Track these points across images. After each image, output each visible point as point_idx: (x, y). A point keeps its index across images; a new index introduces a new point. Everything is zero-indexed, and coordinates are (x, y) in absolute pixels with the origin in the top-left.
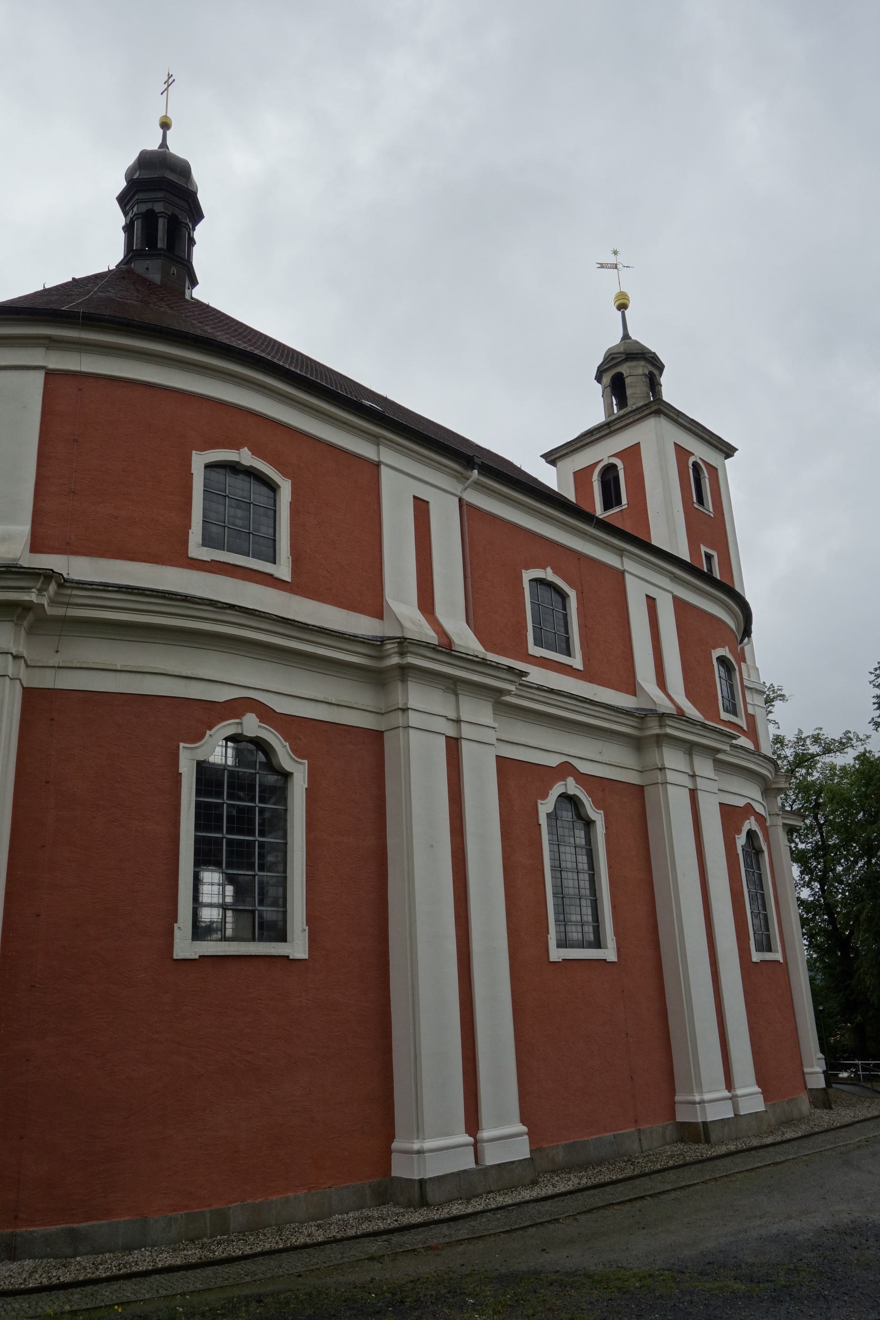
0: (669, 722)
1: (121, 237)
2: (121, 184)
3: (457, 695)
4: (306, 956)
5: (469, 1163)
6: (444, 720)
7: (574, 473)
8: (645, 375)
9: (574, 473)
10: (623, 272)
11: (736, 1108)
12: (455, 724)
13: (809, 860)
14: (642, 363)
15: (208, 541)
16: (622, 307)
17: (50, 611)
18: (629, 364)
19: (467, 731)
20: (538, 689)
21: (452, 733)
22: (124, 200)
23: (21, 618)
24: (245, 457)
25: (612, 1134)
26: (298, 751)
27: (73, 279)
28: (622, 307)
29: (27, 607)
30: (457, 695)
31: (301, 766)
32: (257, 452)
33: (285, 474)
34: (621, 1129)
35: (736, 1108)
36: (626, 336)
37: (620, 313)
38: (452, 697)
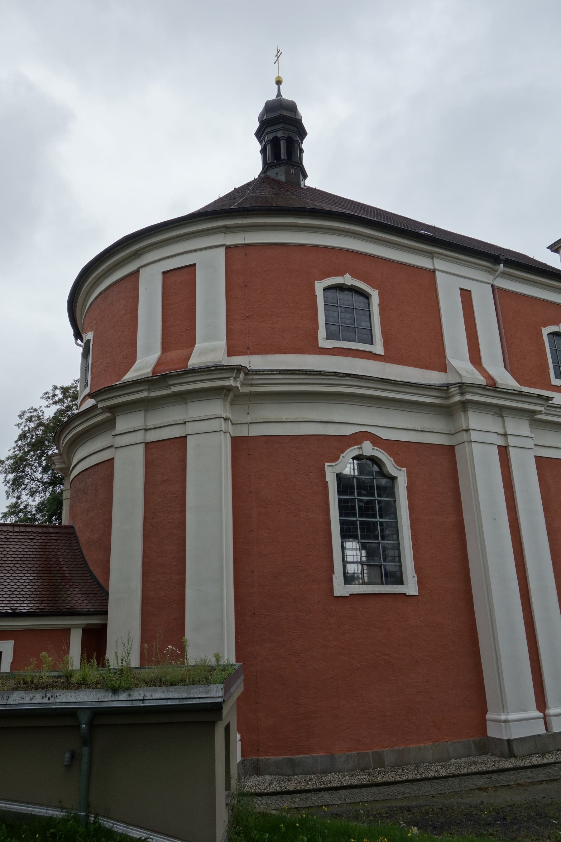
3: (502, 417)
6: (495, 435)
12: (503, 437)
15: (330, 336)
17: (242, 390)
19: (512, 441)
21: (501, 443)
23: (226, 395)
24: (348, 280)
26: (399, 463)
29: (228, 389)
32: (355, 276)
38: (500, 419)
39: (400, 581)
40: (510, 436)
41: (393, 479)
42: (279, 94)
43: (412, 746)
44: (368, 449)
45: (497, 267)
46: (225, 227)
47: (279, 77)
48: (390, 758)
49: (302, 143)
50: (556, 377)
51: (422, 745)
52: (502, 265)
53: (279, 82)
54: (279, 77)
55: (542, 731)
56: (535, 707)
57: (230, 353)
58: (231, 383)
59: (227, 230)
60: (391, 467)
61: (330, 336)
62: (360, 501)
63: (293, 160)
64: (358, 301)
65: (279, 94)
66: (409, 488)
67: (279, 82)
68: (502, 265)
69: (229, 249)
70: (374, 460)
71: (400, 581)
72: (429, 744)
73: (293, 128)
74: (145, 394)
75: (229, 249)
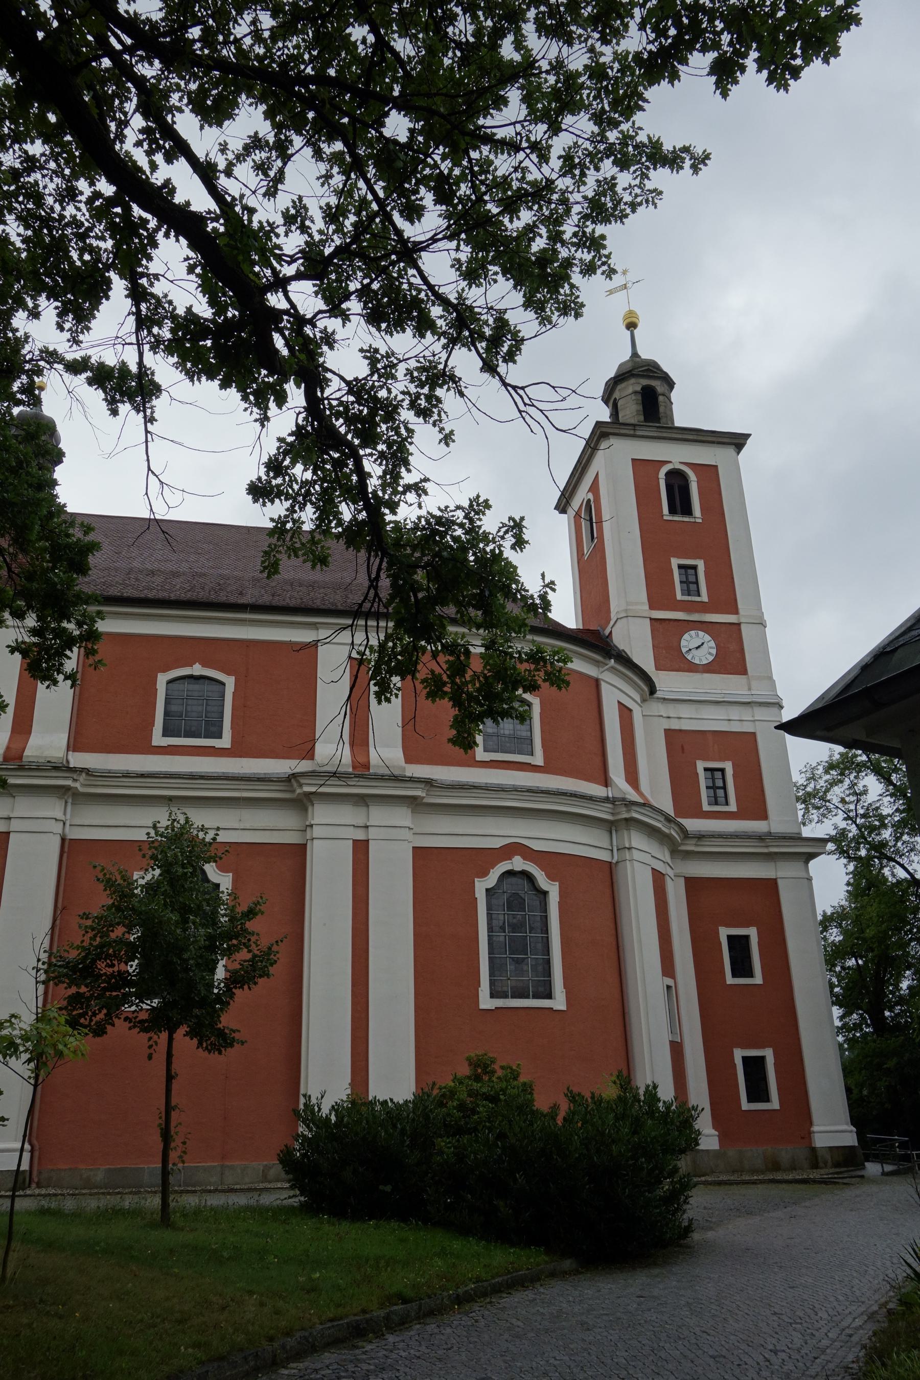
0: (302, 781)
3: (368, 806)
7: (716, 467)
8: (635, 392)
9: (716, 467)
10: (633, 290)
12: (363, 829)
14: (633, 381)
15: (166, 733)
16: (631, 326)
17: (81, 789)
18: (619, 387)
19: (373, 833)
20: (123, 776)
21: (360, 835)
23: (64, 794)
24: (197, 669)
26: (551, 877)
27: (840, 47)
28: (631, 326)
29: (67, 789)
32: (205, 665)
36: (635, 354)
37: (629, 332)
38: (365, 809)
39: (549, 996)
41: (545, 893)
44: (518, 863)
45: (607, 662)
52: (613, 661)
57: (75, 744)
58: (69, 783)
60: (542, 881)
61: (166, 733)
63: (680, 421)
64: (216, 687)
66: (560, 904)
68: (613, 661)
70: (526, 875)
71: (549, 996)
74: (659, 825)
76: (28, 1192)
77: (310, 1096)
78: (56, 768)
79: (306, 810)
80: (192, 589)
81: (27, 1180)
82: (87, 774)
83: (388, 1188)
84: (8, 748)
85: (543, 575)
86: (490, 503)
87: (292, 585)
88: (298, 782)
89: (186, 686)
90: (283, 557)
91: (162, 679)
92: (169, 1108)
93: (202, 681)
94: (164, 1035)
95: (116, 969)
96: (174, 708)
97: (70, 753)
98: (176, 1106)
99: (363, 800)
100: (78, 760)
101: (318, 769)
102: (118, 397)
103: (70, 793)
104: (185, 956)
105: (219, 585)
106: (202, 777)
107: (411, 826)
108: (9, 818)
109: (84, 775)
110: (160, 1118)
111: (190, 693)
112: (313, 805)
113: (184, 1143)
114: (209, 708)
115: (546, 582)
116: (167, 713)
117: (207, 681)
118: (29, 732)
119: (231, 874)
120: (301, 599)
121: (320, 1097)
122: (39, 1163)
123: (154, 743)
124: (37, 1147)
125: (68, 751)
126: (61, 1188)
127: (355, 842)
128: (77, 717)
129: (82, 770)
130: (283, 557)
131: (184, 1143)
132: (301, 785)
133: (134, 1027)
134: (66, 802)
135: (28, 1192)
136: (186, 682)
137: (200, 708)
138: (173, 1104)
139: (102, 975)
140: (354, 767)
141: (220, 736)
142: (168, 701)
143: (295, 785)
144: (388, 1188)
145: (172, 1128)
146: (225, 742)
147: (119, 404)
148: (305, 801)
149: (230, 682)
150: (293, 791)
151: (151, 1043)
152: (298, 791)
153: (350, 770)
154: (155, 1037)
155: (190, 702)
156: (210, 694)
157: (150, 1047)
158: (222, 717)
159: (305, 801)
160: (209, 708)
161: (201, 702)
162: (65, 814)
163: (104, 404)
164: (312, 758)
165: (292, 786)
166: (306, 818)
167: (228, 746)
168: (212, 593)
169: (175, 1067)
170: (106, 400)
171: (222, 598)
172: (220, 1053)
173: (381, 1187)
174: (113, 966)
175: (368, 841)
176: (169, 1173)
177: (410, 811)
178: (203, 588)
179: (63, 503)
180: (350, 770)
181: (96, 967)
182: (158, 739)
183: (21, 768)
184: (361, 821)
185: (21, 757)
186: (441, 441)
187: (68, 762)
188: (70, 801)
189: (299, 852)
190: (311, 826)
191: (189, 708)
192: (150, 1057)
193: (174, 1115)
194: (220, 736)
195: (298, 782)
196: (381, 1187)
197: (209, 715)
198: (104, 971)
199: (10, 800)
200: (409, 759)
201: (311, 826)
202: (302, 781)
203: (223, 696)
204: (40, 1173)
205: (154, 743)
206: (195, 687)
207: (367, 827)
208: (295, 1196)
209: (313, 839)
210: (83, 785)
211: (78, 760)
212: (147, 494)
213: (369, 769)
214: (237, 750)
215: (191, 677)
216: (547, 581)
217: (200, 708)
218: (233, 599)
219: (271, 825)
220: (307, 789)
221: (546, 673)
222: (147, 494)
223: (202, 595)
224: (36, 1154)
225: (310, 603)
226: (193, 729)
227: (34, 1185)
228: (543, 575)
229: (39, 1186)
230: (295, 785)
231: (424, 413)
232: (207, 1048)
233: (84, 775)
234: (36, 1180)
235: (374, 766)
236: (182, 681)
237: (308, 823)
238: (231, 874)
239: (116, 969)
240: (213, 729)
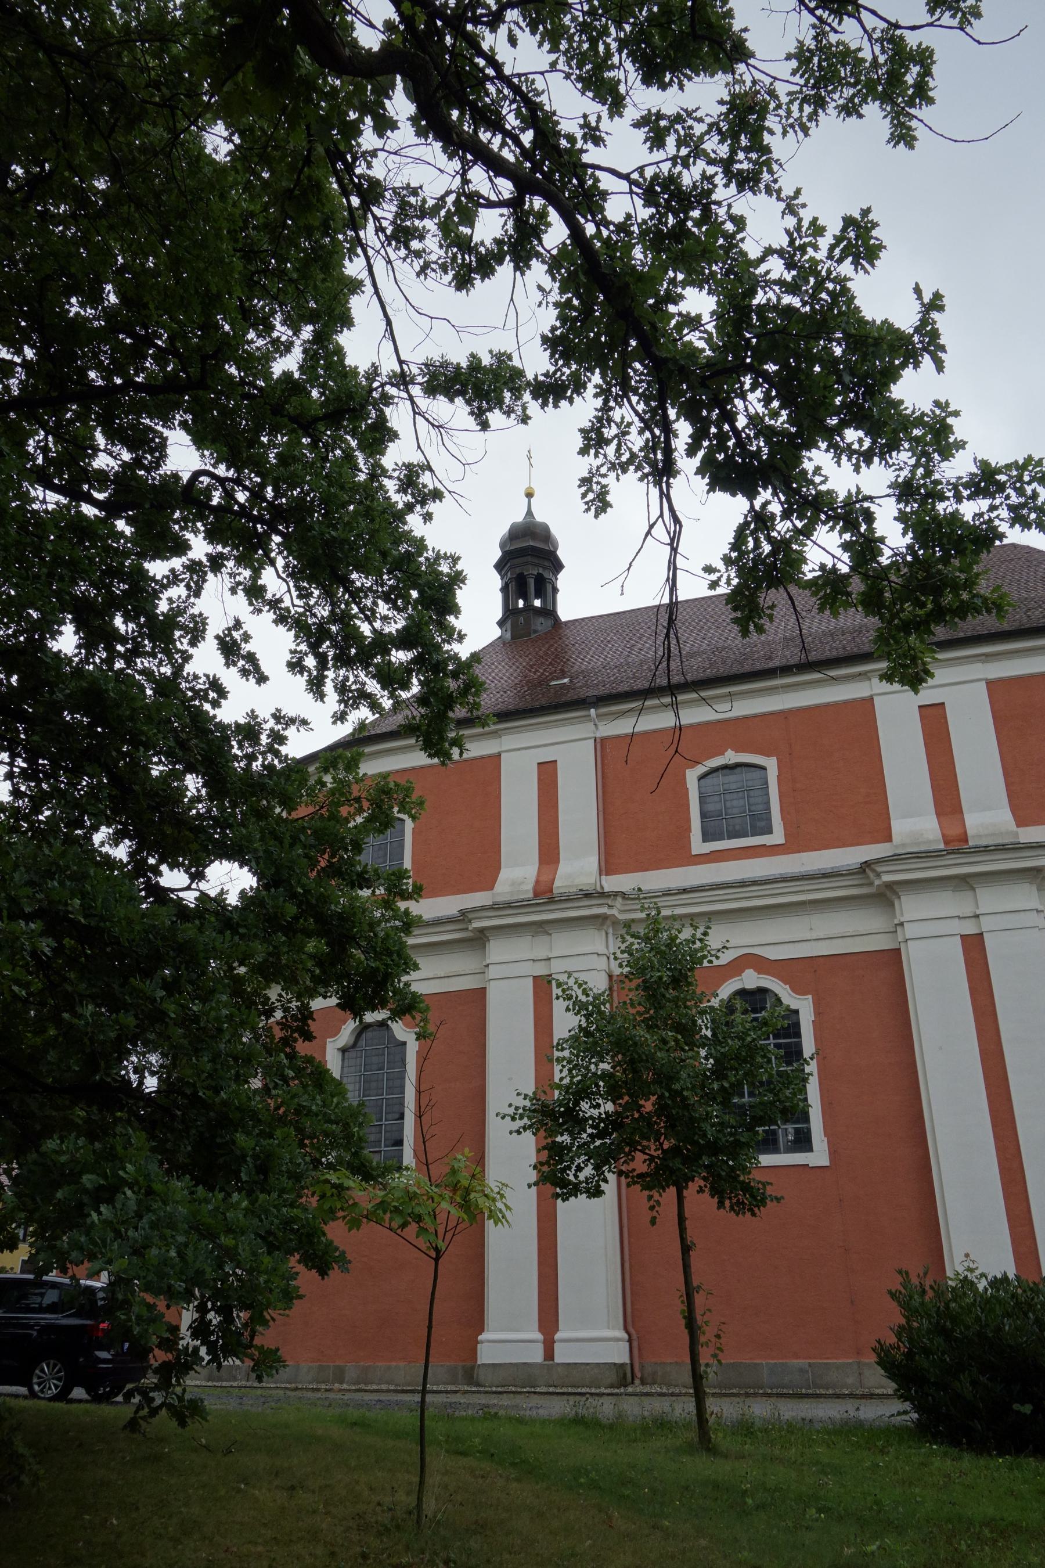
0: (879, 869)
1: (499, 597)
2: (498, 554)
3: (974, 889)
4: (828, 1164)
5: (536, 1356)
6: (957, 919)
11: (549, 1354)
12: (973, 920)
13: (720, 347)
15: (707, 837)
17: (621, 917)
19: (986, 924)
21: (970, 928)
22: (499, 566)
23: (602, 924)
24: (731, 757)
25: (808, 1361)
26: (798, 990)
30: (974, 889)
31: (805, 1002)
33: (768, 754)
34: (828, 1358)
35: (549, 1354)
38: (970, 893)
40: (910, 924)
42: (529, 513)
43: (380, 1364)
46: (986, 655)
47: (530, 487)
48: (351, 1373)
49: (557, 579)
50: (491, 888)
51: (394, 1364)
53: (529, 495)
54: (530, 487)
55: (536, 1356)
56: (536, 1325)
57: (607, 867)
58: (604, 910)
59: (988, 657)
60: (789, 998)
61: (707, 837)
62: (777, 1046)
64: (756, 774)
65: (529, 513)
67: (529, 495)
69: (992, 686)
72: (402, 1364)
73: (546, 563)
75: (992, 686)
76: (630, 1389)
77: (907, 1273)
78: (587, 895)
79: (892, 905)
80: (712, 665)
81: (629, 1375)
82: (624, 898)
83: (1027, 1409)
84: (537, 882)
85: (918, 290)
86: (820, 222)
87: (832, 635)
88: (874, 871)
89: (719, 779)
90: (610, 480)
91: (692, 776)
92: (690, 1292)
93: (739, 770)
94: (672, 1190)
95: (602, 1110)
96: (710, 807)
97: (603, 877)
98: (699, 1287)
99: (965, 882)
100: (612, 883)
101: (898, 852)
102: (484, 404)
103: (608, 922)
104: (677, 1086)
105: (744, 654)
106: (754, 883)
107: (1040, 908)
108: (549, 959)
109: (619, 899)
110: (683, 1302)
111: (726, 787)
112: (899, 898)
113: (718, 1336)
114: (752, 800)
115: (926, 300)
116: (704, 815)
117: (744, 769)
118: (557, 861)
119: (810, 996)
120: (844, 648)
121: (921, 1275)
122: (640, 1356)
123: (695, 851)
124: (634, 1336)
125: (600, 875)
126: (669, 1385)
127: (964, 938)
128: (605, 837)
129: (616, 894)
130: (610, 480)
131: (718, 1336)
132: (878, 875)
133: (635, 1183)
134: (607, 934)
135: (630, 1389)
136: (720, 773)
137: (741, 802)
138: (695, 1284)
139: (586, 1120)
140: (946, 843)
141: (769, 831)
142: (702, 799)
143: (871, 875)
144: (1027, 1409)
145: (699, 1318)
146: (777, 836)
147: (488, 414)
148: (888, 893)
149: (771, 764)
150: (871, 884)
151: (652, 1203)
152: (877, 882)
153: (942, 846)
154: (656, 1196)
155: (728, 797)
156: (750, 783)
157: (652, 1208)
158: (769, 808)
159: (888, 893)
160: (752, 800)
161: (740, 794)
162: (607, 947)
163: (472, 419)
164: (889, 838)
165: (868, 877)
166: (894, 916)
167: (782, 841)
168: (735, 664)
169: (692, 1233)
170: (472, 413)
171: (747, 667)
172: (754, 1214)
173: (1016, 1407)
174: (598, 1106)
175: (982, 934)
176: (701, 1377)
177: (1034, 888)
178: (724, 663)
179: (419, 536)
180: (942, 846)
181: (580, 1110)
182: (698, 846)
183: (551, 901)
184: (968, 911)
185: (551, 891)
186: (783, 213)
187: (602, 887)
188: (611, 931)
189: (893, 957)
190: (902, 924)
191: (728, 804)
192: (653, 1221)
193: (699, 1299)
194: (769, 831)
195: (874, 871)
196: (1016, 1407)
197: (753, 808)
198: (589, 1114)
199: (546, 938)
200: (1021, 822)
201: (902, 924)
202: (879, 869)
203: (766, 783)
204: (642, 1368)
205: (695, 851)
206: (732, 780)
207: (977, 916)
208: (905, 1412)
209: (906, 941)
210: (621, 911)
211: (612, 883)
212: (419, 447)
213: (966, 841)
214: (793, 845)
215: (726, 767)
216: (927, 298)
217: (741, 802)
218: (759, 666)
219: (851, 930)
220: (887, 878)
221: (1011, 508)
222: (419, 447)
223: (723, 670)
224: (635, 1344)
225: (856, 650)
226: (737, 827)
227: (637, 1382)
228: (918, 290)
229: (643, 1382)
230: (871, 875)
231: (747, 182)
232: (732, 1208)
233: (619, 899)
234: (639, 1375)
235: (973, 837)
236: (714, 775)
237: (896, 922)
238: (810, 996)
239: (602, 1110)
240: (763, 824)
